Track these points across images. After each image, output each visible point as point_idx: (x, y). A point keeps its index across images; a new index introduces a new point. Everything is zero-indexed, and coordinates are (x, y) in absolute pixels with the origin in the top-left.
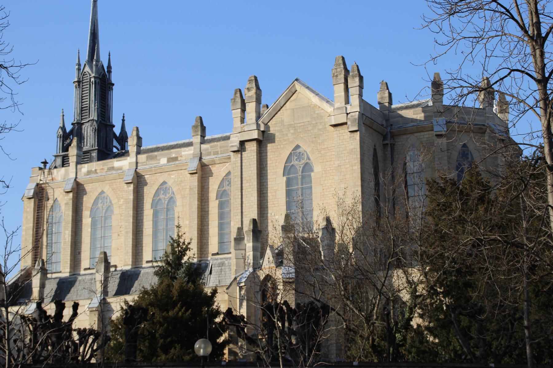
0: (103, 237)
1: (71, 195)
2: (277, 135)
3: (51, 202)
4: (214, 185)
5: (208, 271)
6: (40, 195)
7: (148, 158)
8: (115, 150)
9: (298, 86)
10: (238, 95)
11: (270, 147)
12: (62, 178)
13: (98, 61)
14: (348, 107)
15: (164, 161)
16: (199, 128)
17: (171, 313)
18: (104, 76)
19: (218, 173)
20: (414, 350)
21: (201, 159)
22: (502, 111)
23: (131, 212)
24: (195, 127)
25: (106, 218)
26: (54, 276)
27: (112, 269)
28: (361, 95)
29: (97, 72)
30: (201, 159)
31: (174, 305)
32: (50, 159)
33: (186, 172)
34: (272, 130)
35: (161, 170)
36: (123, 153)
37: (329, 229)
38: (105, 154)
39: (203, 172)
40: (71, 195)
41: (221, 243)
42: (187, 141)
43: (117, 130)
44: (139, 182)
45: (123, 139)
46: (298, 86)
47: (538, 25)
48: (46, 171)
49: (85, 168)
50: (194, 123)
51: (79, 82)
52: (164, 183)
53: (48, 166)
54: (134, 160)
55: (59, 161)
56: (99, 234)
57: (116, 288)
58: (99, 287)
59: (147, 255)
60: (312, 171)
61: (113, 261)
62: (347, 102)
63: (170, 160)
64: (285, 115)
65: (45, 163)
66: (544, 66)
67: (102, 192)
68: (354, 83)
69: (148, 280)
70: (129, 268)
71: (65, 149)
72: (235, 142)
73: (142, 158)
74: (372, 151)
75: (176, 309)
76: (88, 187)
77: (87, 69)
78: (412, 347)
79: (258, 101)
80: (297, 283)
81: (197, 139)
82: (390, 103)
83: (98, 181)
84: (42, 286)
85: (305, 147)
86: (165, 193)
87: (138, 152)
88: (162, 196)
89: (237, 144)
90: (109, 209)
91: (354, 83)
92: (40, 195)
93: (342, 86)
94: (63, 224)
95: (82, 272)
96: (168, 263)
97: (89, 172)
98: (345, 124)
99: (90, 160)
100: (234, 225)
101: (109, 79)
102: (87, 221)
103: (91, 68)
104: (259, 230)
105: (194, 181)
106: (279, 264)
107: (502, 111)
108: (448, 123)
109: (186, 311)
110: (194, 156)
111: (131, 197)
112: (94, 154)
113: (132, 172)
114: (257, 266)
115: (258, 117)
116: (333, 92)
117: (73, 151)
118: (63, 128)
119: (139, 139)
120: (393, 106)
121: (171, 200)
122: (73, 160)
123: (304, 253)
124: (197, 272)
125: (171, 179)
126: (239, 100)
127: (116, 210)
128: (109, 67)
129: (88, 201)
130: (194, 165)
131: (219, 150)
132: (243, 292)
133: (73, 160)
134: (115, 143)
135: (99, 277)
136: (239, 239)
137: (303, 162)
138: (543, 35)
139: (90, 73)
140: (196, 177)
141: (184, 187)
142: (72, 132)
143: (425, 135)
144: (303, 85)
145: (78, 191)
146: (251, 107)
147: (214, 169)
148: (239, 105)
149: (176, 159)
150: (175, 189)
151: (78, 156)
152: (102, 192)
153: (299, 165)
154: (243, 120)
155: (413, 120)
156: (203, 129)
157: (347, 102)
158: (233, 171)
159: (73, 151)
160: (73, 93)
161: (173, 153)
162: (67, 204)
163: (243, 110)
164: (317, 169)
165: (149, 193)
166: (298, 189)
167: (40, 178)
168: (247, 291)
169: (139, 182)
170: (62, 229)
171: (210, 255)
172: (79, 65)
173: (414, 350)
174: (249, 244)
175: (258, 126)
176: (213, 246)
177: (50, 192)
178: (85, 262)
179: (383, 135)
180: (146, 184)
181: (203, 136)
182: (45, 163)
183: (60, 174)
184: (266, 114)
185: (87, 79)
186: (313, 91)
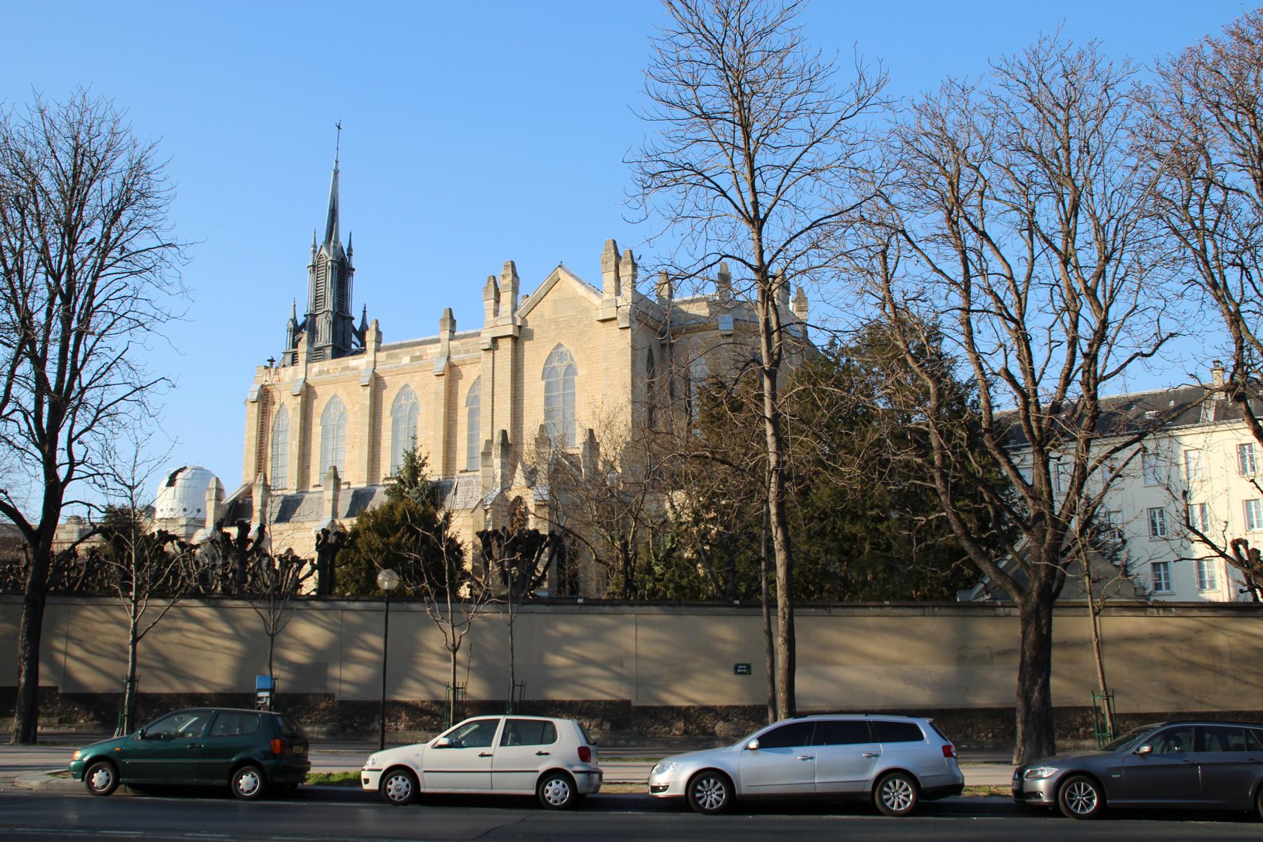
0: (335, 449)
1: (299, 398)
2: (536, 331)
3: (277, 406)
4: (463, 388)
5: (453, 491)
6: (265, 398)
7: (388, 357)
8: (354, 347)
9: (561, 274)
10: (492, 283)
11: (527, 345)
12: (290, 379)
13: (336, 242)
14: (619, 299)
15: (406, 360)
16: (448, 322)
17: (392, 539)
18: (343, 259)
19: (469, 374)
20: (671, 585)
21: (449, 358)
22: (800, 310)
23: (367, 420)
24: (443, 320)
25: (339, 427)
26: (280, 492)
27: (343, 487)
28: (634, 287)
29: (335, 255)
30: (449, 358)
31: (397, 529)
32: (278, 357)
33: (431, 375)
34: (530, 325)
35: (402, 371)
36: (362, 351)
37: (592, 443)
38: (341, 350)
39: (452, 373)
40: (299, 398)
41: (471, 458)
42: (436, 337)
43: (357, 324)
44: (377, 384)
45: (361, 335)
46: (561, 274)
47: (756, 204)
48: (272, 370)
49: (316, 367)
50: (442, 315)
51: (314, 266)
52: (406, 386)
53: (275, 364)
54: (372, 358)
55: (289, 358)
56: (330, 445)
57: (347, 509)
58: (328, 507)
59: (386, 469)
60: (576, 374)
61: (344, 477)
62: (618, 293)
63: (414, 359)
64: (545, 307)
65: (272, 361)
66: (761, 252)
67: (335, 396)
68: (626, 271)
69: (380, 500)
70: (364, 485)
71: (295, 345)
72: (486, 340)
73: (382, 356)
74: (646, 352)
75: (399, 535)
76: (319, 390)
77: (324, 251)
78: (670, 581)
79: (515, 290)
80: (550, 506)
81: (446, 335)
82: (671, 296)
83: (331, 382)
84: (264, 505)
85: (568, 346)
86: (407, 399)
87: (377, 350)
88: (403, 402)
89: (489, 341)
90: (342, 415)
91: (626, 271)
92: (265, 398)
93: (612, 275)
94: (290, 433)
95: (311, 489)
96: (401, 481)
97: (321, 373)
98: (615, 319)
99: (324, 358)
100: (484, 435)
101: (349, 263)
102: (317, 429)
103: (328, 250)
104: (509, 447)
105: (441, 384)
106: (531, 484)
107: (800, 310)
108: (736, 320)
109: (411, 536)
110: (442, 354)
111: (368, 402)
112: (329, 351)
113: (370, 373)
114: (506, 486)
115: (515, 309)
116: (602, 282)
117: (303, 348)
118: (294, 321)
119: (379, 333)
120: (676, 300)
121: (414, 406)
122: (302, 357)
123: (561, 474)
124: (436, 493)
125: (415, 381)
126: (492, 289)
127: (350, 418)
128: (350, 249)
129: (318, 406)
130: (441, 365)
131: (470, 347)
132: (489, 516)
133: (302, 357)
134: (354, 338)
135: (329, 494)
136: (487, 454)
137: (565, 363)
138: (762, 216)
139: (327, 256)
140: (442, 379)
141: (429, 391)
142: (304, 325)
143: (712, 334)
144: (568, 272)
145: (307, 394)
146: (506, 297)
147: (465, 370)
148: (492, 295)
149: (420, 358)
150: (418, 394)
151: (308, 353)
152: (335, 396)
153: (560, 366)
154: (496, 313)
155: (696, 317)
156: (453, 322)
157: (618, 293)
158: (484, 373)
159: (303, 348)
160: (308, 279)
161: (417, 351)
162: (294, 409)
163: (497, 301)
164: (582, 372)
165: (388, 397)
166: (558, 396)
167: (266, 378)
168: (493, 515)
169: (377, 384)
170: (289, 439)
171: (457, 473)
172: (315, 246)
173: (671, 585)
174: (497, 461)
175: (514, 319)
176: (461, 462)
177: (276, 395)
178: (314, 478)
179: (658, 335)
180: (385, 387)
181: (452, 331)
182: (272, 361)
183: (288, 374)
184: (523, 305)
185: (322, 263)
186: (579, 280)
